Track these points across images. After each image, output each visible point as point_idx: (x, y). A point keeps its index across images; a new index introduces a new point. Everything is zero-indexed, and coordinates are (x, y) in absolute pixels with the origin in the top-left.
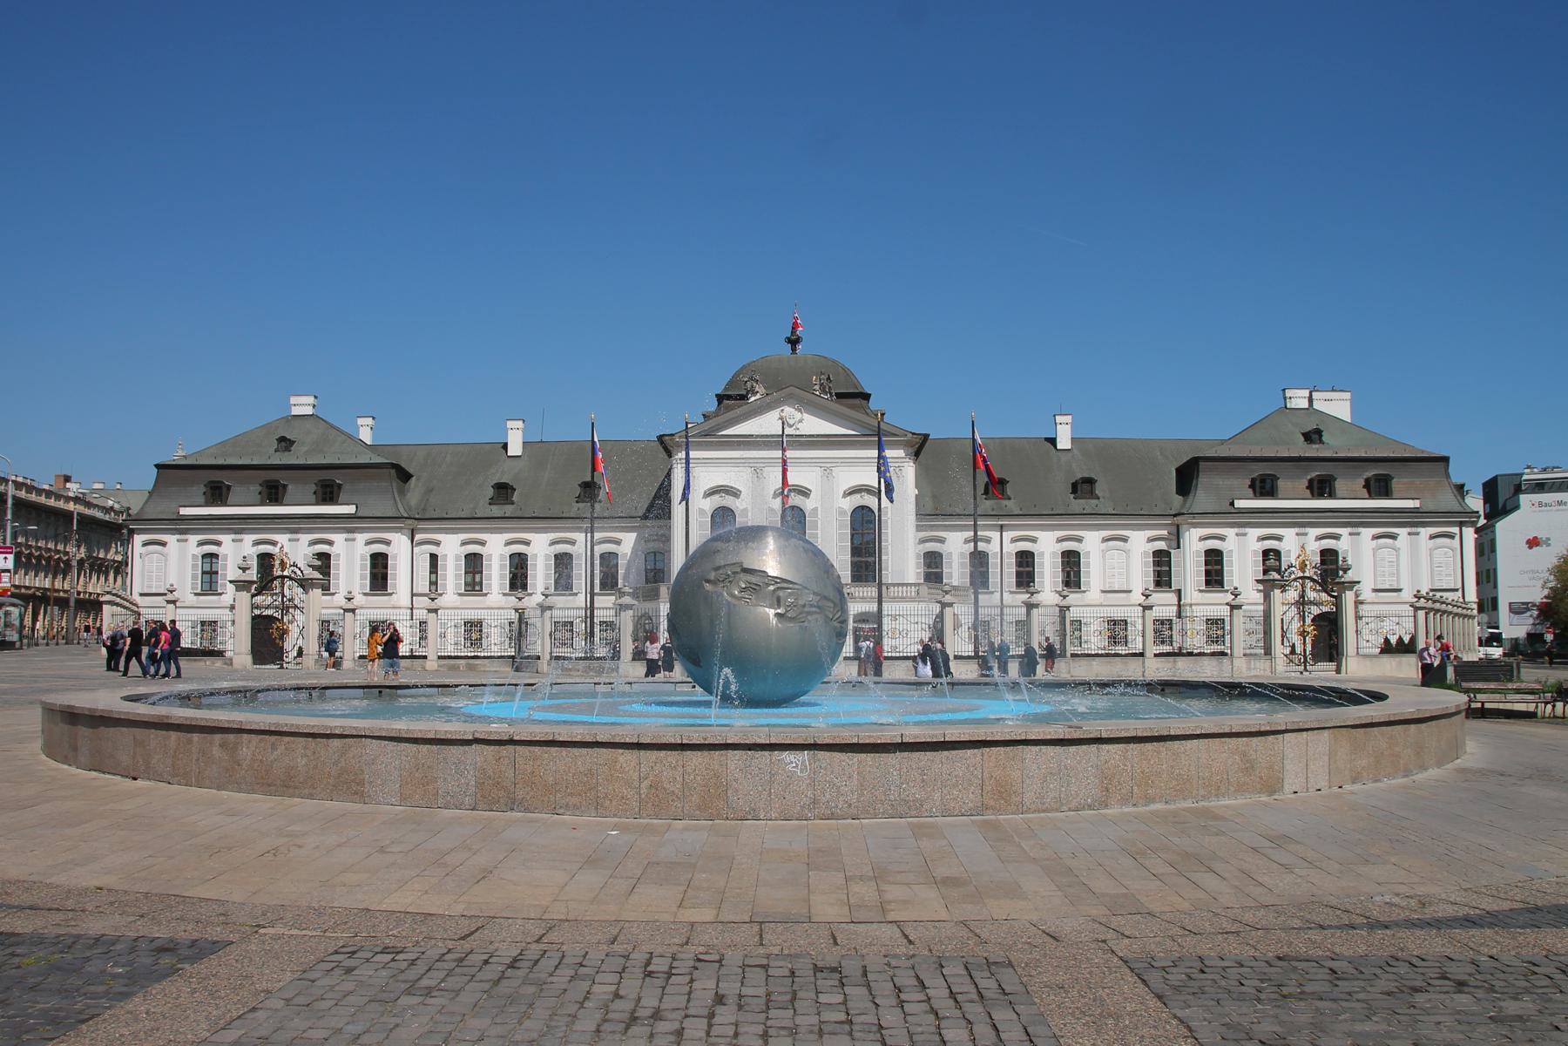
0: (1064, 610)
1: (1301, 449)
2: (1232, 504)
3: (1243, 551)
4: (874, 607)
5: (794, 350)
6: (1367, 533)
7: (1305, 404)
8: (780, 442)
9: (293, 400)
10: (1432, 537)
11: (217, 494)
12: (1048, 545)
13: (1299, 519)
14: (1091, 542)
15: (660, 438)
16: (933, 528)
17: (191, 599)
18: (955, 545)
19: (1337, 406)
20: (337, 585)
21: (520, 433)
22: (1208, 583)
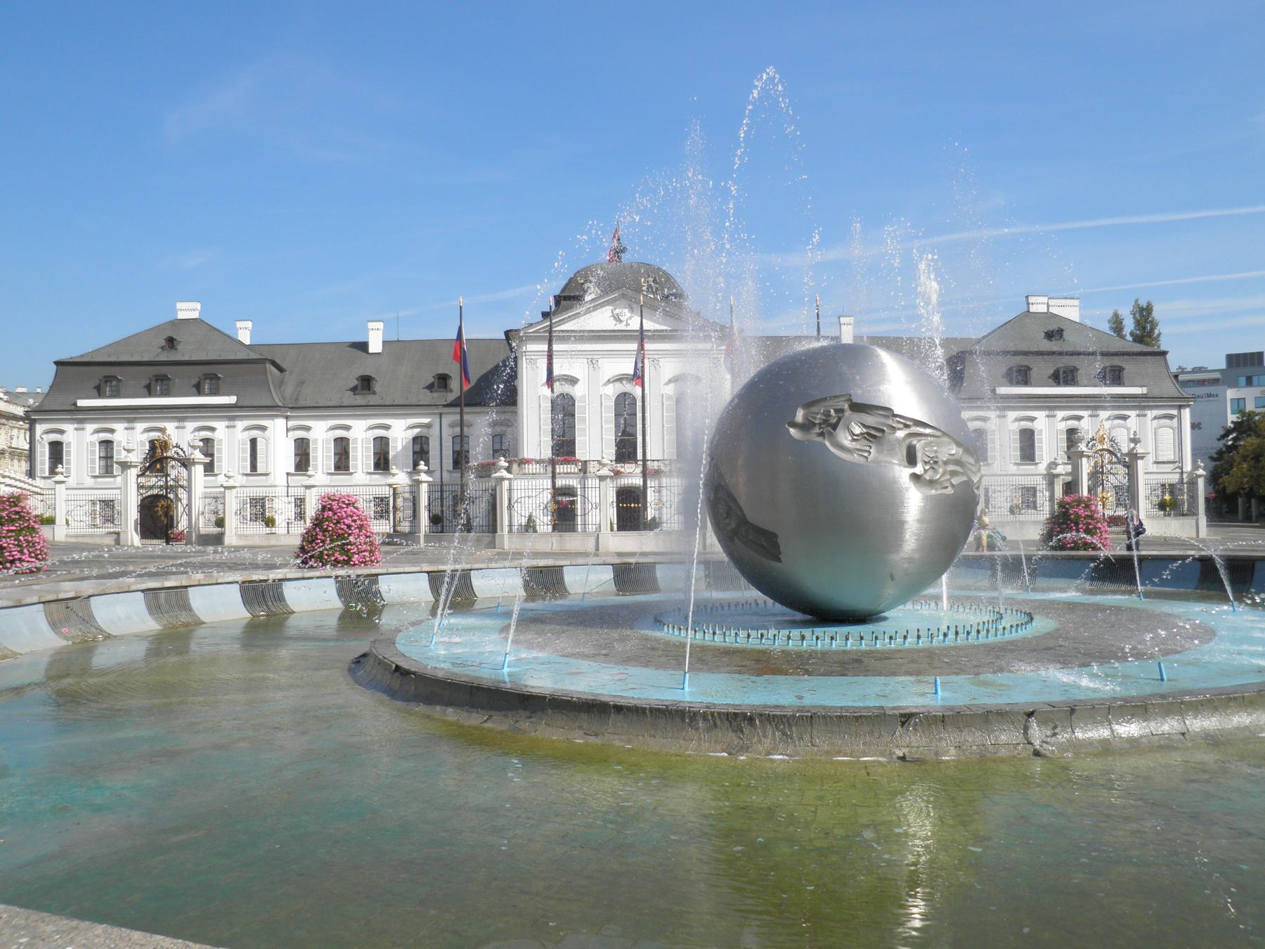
1: (1047, 346)
2: (75, 404)
9: (179, 305)
10: (1155, 418)
16: (1119, 408)
17: (239, 480)
19: (1070, 311)
20: (356, 466)
21: (380, 332)
22: (337, 468)
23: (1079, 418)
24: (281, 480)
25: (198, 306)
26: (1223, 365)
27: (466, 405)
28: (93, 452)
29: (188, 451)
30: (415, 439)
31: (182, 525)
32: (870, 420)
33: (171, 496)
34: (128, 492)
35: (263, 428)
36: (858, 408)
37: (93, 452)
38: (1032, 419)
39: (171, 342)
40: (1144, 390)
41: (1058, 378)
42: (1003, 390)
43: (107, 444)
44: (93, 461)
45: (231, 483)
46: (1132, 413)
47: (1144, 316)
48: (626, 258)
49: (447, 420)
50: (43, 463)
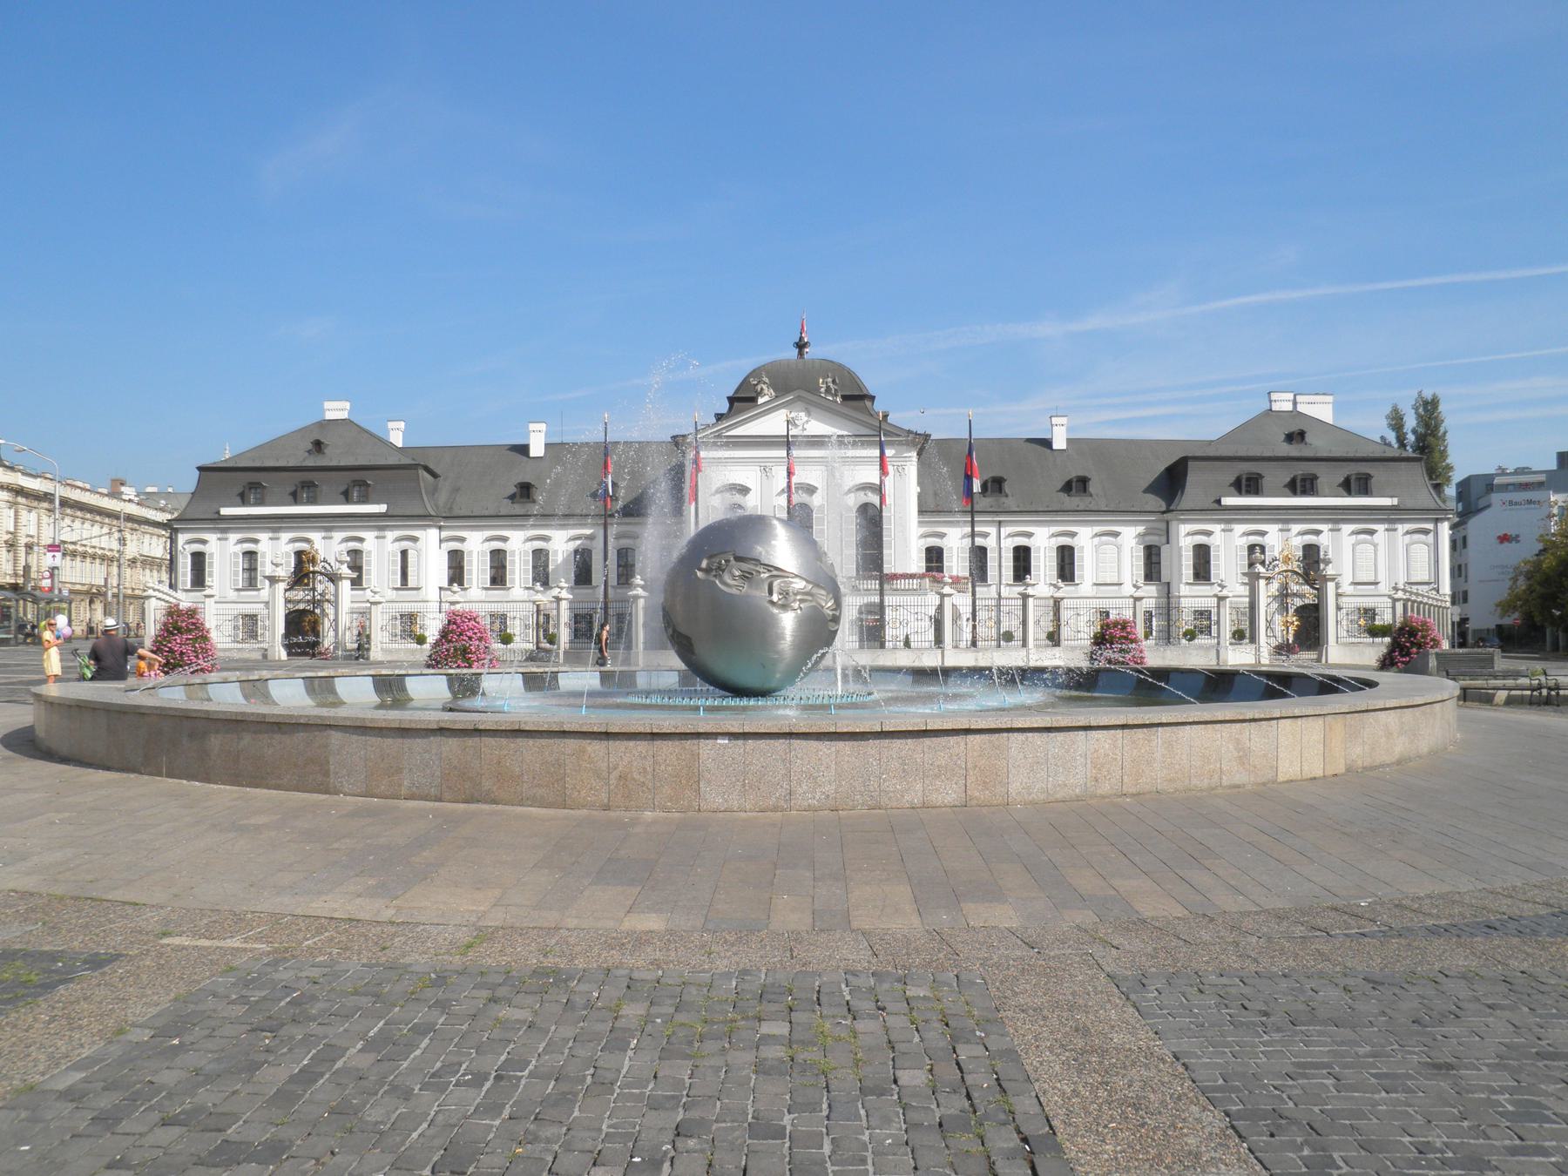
0: (1057, 603)
2: (1219, 502)
3: (1229, 544)
4: (877, 599)
5: (801, 354)
6: (1347, 528)
8: (787, 443)
9: (327, 405)
10: (1408, 533)
12: (1043, 541)
13: (1283, 516)
14: (1085, 538)
18: (955, 542)
19: (1320, 409)
20: (513, 581)
23: (1318, 533)
24: (432, 594)
25: (347, 405)
26: (1553, 465)
28: (236, 564)
29: (336, 565)
30: (576, 552)
31: (328, 641)
33: (318, 611)
34: (274, 605)
35: (415, 539)
37: (236, 564)
38: (1209, 533)
39: (318, 446)
40: (1395, 501)
41: (1294, 487)
42: (1228, 501)
43: (250, 555)
44: (236, 574)
45: (377, 598)
46: (1380, 528)
47: (1429, 410)
50: (184, 575)
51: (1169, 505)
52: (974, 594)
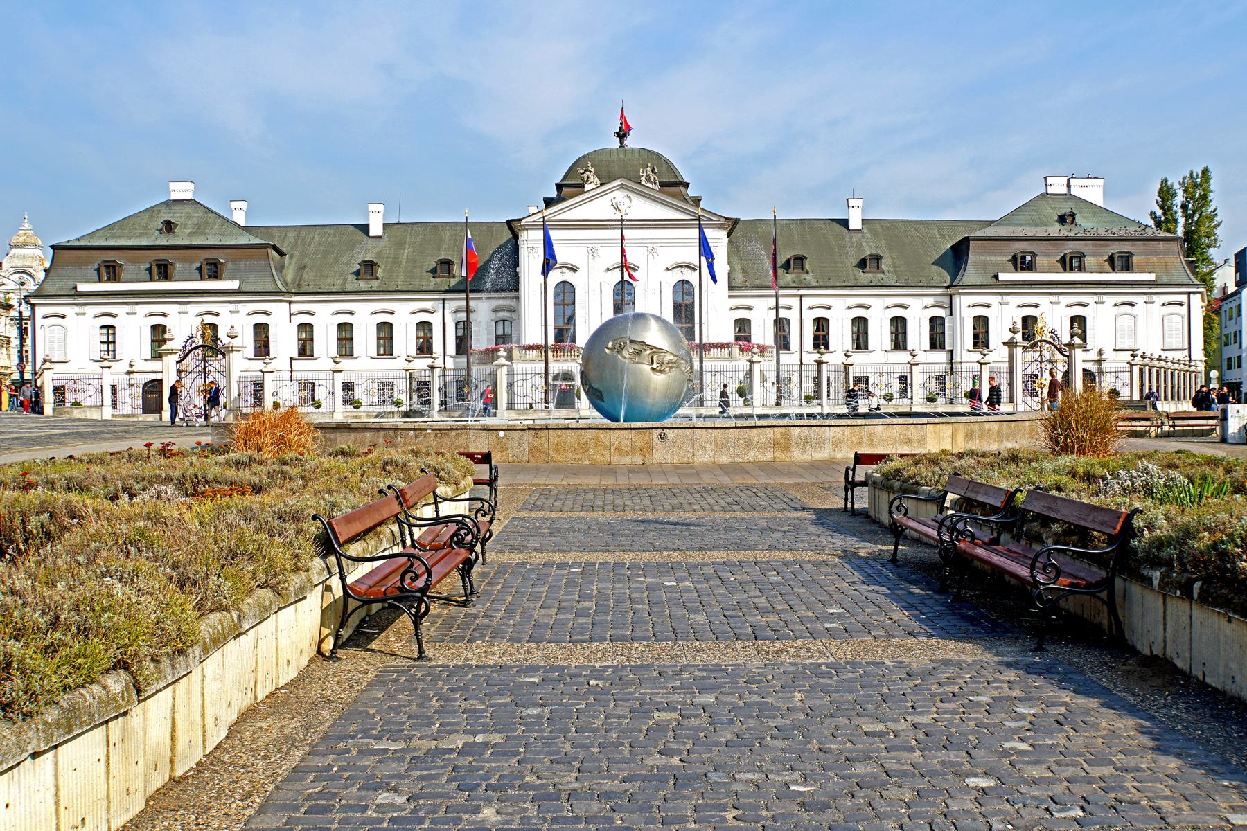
1: (1055, 230)
2: (996, 277)
3: (1004, 315)
7: (1064, 190)
8: (622, 224)
9: (172, 186)
11: (111, 271)
15: (509, 223)
19: (1091, 192)
25: (190, 186)
27: (473, 291)
32: (636, 347)
36: (632, 342)
39: (169, 226)
41: (1067, 263)
47: (1198, 189)
48: (628, 142)
49: (450, 305)
51: (954, 277)
52: (778, 362)
